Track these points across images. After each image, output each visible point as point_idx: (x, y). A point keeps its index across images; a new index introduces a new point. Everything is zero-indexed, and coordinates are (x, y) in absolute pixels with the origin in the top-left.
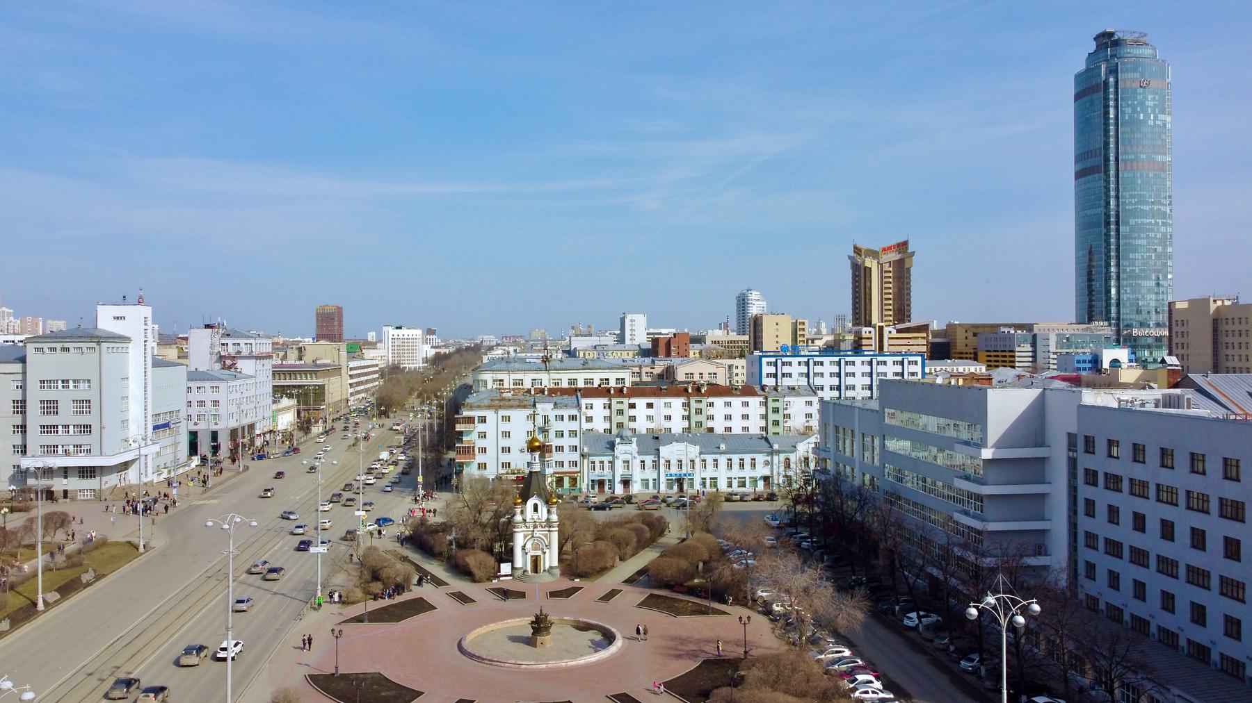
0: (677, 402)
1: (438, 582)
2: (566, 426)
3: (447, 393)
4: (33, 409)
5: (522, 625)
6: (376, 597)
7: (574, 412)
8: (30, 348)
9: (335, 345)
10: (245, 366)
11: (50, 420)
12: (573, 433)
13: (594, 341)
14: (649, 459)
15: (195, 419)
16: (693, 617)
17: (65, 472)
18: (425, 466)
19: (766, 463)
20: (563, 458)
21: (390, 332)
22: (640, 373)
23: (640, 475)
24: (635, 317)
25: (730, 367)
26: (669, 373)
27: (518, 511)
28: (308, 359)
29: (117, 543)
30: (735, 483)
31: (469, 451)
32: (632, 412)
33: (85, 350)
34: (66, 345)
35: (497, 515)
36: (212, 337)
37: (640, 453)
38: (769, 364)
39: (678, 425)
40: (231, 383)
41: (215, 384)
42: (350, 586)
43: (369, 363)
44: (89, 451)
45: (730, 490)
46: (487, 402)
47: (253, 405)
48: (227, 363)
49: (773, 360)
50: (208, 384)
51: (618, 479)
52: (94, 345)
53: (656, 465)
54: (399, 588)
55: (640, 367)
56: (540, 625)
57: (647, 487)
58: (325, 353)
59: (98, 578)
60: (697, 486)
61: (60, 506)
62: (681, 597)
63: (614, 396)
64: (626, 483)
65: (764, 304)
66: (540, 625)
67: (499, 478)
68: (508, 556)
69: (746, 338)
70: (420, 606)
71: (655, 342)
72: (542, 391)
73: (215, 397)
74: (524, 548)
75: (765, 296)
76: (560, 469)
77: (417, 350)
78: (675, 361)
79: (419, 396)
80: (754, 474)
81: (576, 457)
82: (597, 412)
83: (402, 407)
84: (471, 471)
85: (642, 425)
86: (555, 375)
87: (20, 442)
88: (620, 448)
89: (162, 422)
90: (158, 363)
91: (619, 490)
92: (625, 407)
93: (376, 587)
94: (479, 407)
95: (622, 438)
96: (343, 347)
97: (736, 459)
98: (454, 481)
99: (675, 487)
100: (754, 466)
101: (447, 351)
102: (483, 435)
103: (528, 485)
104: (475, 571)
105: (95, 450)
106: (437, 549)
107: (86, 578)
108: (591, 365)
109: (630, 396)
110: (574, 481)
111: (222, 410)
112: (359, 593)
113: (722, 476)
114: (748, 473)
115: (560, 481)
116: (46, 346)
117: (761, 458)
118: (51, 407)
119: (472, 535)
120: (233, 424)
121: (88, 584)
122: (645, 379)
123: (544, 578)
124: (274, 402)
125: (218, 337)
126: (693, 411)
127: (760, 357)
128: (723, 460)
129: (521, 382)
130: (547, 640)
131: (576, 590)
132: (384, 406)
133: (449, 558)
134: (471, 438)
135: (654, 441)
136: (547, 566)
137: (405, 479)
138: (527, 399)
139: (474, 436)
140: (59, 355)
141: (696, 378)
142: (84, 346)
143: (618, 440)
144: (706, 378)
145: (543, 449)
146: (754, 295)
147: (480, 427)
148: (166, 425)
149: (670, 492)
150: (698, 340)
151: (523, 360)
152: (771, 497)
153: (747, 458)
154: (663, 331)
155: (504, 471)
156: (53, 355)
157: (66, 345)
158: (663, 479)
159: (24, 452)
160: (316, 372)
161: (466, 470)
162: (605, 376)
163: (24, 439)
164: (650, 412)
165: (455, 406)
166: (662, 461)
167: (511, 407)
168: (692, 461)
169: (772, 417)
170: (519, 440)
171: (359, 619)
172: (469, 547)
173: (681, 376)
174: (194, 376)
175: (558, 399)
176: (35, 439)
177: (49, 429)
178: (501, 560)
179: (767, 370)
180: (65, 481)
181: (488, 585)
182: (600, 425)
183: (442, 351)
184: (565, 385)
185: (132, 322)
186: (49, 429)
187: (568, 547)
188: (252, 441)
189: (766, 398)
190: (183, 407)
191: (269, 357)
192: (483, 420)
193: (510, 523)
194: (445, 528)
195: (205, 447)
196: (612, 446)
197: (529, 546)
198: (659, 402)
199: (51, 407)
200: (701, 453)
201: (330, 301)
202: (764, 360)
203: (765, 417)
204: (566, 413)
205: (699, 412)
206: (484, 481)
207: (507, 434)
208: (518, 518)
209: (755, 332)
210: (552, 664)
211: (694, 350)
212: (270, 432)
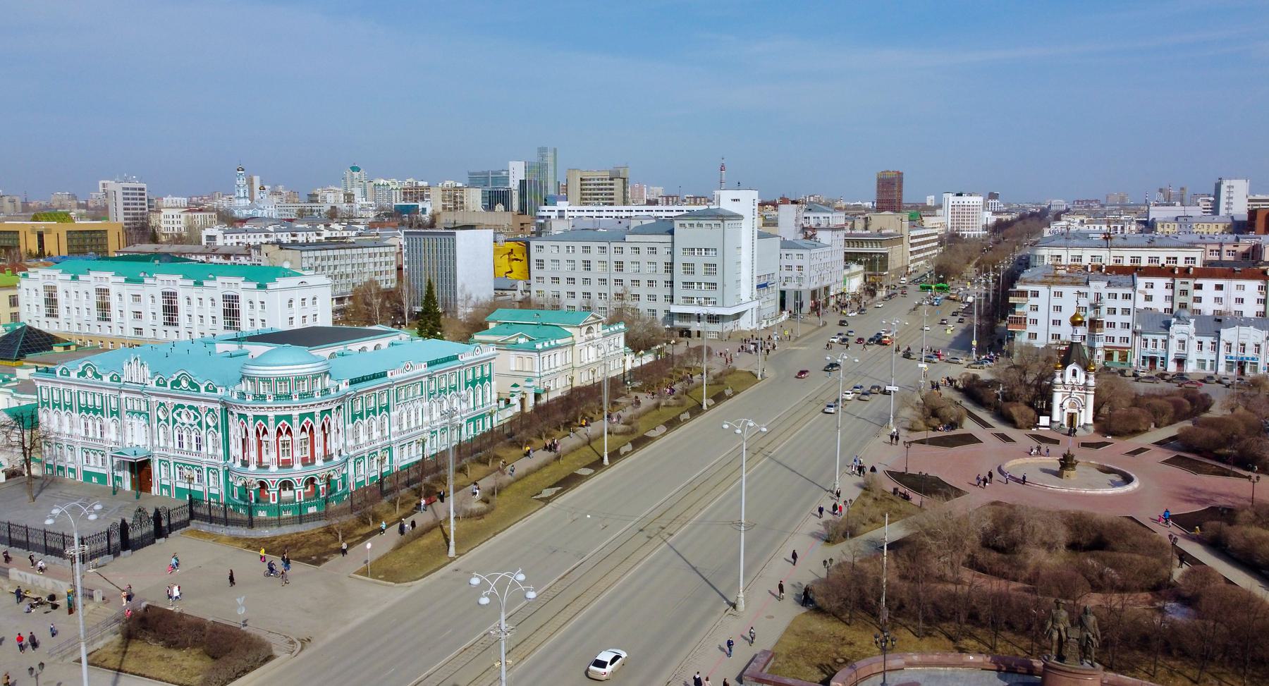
1: (985, 425)
2: (1120, 304)
3: (1005, 265)
4: (678, 269)
5: (1053, 462)
6: (935, 429)
7: (1128, 291)
8: (677, 223)
9: (899, 215)
10: (823, 236)
11: (689, 278)
12: (1126, 311)
13: (1177, 210)
14: (1207, 341)
18: (980, 332)
20: (1115, 333)
21: (951, 199)
22: (1220, 252)
23: (1196, 355)
24: (1234, 182)
27: (1058, 374)
28: (873, 228)
29: (742, 372)
31: (1021, 321)
32: (1197, 293)
35: (1041, 378)
36: (797, 211)
37: (1197, 334)
39: (1251, 308)
40: (813, 251)
41: (800, 252)
42: (916, 419)
43: (929, 231)
44: (715, 303)
46: (1040, 278)
48: (809, 233)
50: (794, 252)
51: (1171, 357)
53: (1215, 347)
54: (953, 425)
55: (1221, 245)
56: (1067, 462)
57: (1203, 367)
58: (887, 222)
59: (735, 393)
61: (694, 343)
62: (1207, 461)
64: (1180, 362)
66: (1067, 462)
67: (1048, 347)
68: (1048, 411)
70: (969, 439)
71: (1253, 214)
72: (1100, 269)
73: (800, 262)
74: (1061, 405)
76: (1110, 344)
77: (976, 215)
79: (977, 265)
81: (1128, 333)
82: (1159, 293)
83: (959, 274)
84: (1022, 339)
85: (1208, 307)
86: (1115, 252)
87: (669, 294)
88: (1175, 328)
89: (762, 282)
90: (761, 236)
91: (1172, 368)
93: (935, 422)
94: (1032, 282)
95: (1178, 318)
96: (906, 216)
98: (1005, 347)
99: (1235, 370)
101: (1009, 218)
102: (1035, 308)
103: (1070, 354)
104: (1017, 419)
105: (719, 303)
106: (987, 400)
107: (728, 392)
108: (1157, 242)
110: (1124, 357)
111: (805, 272)
112: (921, 424)
115: (1109, 356)
116: (687, 223)
118: (689, 268)
119: (1016, 391)
120: (813, 286)
121: (730, 397)
122: (1226, 257)
124: (846, 267)
130: (1072, 474)
131: (1106, 444)
132: (943, 274)
133: (996, 408)
134: (1024, 308)
137: (961, 344)
138: (1079, 276)
139: (1026, 309)
142: (713, 222)
145: (1094, 324)
147: (1033, 301)
148: (765, 285)
149: (1229, 374)
151: (1086, 236)
155: (1054, 342)
158: (1222, 360)
159: (672, 301)
160: (880, 241)
161: (1018, 338)
162: (1172, 255)
163: (672, 291)
164: (1219, 294)
165: (1012, 278)
166: (1222, 344)
167: (1063, 284)
171: (922, 442)
172: (1017, 399)
174: (786, 245)
175: (1113, 278)
177: (688, 285)
178: (1041, 413)
181: (1028, 432)
182: (1160, 304)
183: (1005, 217)
184: (1127, 263)
185: (743, 202)
186: (688, 285)
187: (1105, 410)
191: (841, 228)
193: (1050, 388)
194: (993, 384)
195: (790, 304)
196: (1167, 325)
197: (1066, 404)
198: (1230, 285)
199: (689, 268)
201: (892, 167)
206: (1030, 348)
207: (1059, 308)
208: (1058, 380)
210: (1073, 490)
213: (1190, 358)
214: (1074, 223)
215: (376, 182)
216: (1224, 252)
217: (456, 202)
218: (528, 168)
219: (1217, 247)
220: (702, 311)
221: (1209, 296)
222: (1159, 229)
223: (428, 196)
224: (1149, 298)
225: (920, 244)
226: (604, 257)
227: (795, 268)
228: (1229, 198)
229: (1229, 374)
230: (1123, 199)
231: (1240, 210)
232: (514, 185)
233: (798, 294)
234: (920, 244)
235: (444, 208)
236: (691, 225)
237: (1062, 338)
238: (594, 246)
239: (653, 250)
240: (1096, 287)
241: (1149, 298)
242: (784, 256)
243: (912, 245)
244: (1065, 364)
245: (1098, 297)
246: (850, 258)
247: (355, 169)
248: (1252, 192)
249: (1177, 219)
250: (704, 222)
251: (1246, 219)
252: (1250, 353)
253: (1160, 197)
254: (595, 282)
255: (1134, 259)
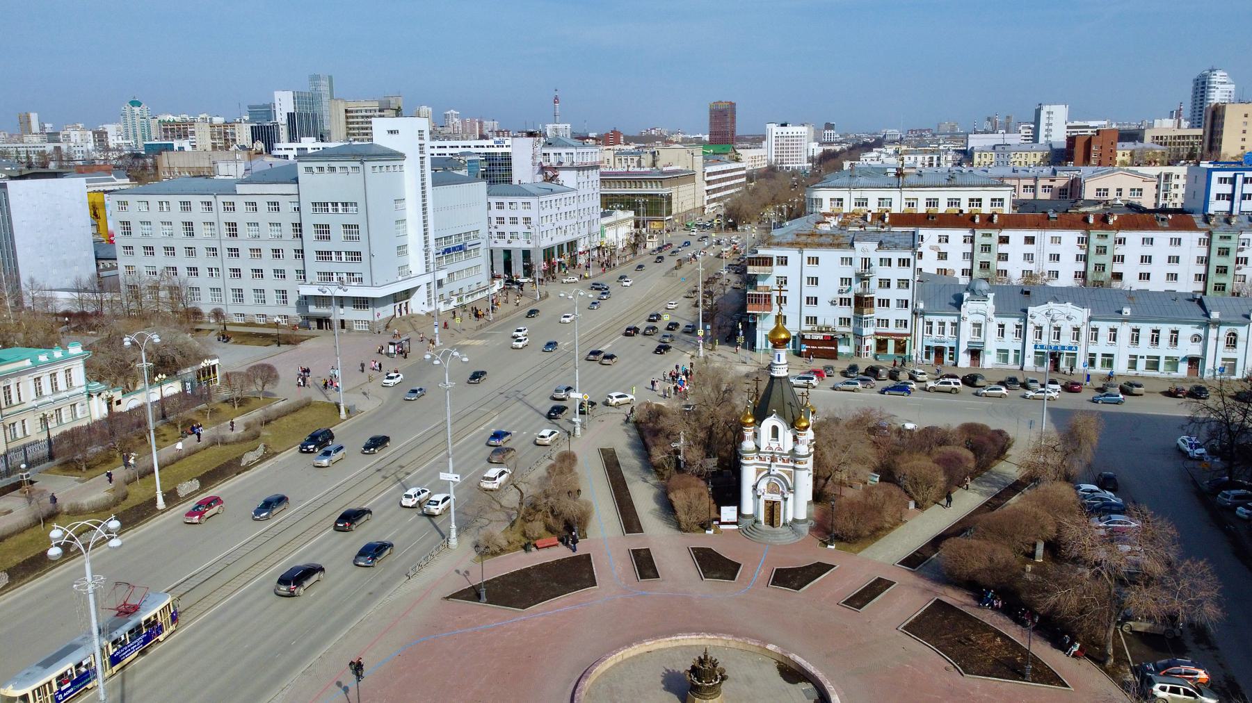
0: (1070, 238)
1: (631, 522)
2: (895, 273)
4: (309, 233)
7: (907, 255)
8: (301, 167)
10: (567, 178)
11: (324, 246)
12: (903, 283)
14: (1011, 323)
15: (508, 236)
16: (994, 681)
17: (342, 301)
19: (1196, 339)
21: (774, 130)
22: (1034, 188)
24: (1053, 108)
25: (1167, 176)
26: (1073, 191)
27: (749, 433)
30: (1141, 364)
32: (1003, 248)
33: (350, 169)
34: (333, 164)
38: (1222, 180)
40: (543, 199)
41: (526, 199)
44: (361, 280)
45: (1132, 372)
46: (790, 238)
47: (574, 221)
49: (1230, 174)
50: (519, 200)
51: (963, 347)
52: (357, 164)
53: (1021, 332)
55: (1036, 179)
57: (1005, 359)
60: (1080, 365)
63: (981, 226)
64: (975, 353)
65: (1232, 87)
68: (734, 498)
69: (1199, 132)
71: (1071, 140)
73: (527, 213)
74: (755, 487)
75: (1234, 77)
78: (1085, 171)
80: (1173, 353)
81: (906, 314)
82: (947, 252)
86: (908, 194)
88: (969, 307)
91: (964, 361)
92: (994, 241)
94: (779, 244)
95: (973, 292)
97: (1146, 330)
99: (1048, 365)
100: (1174, 340)
101: (838, 148)
102: (783, 281)
105: (366, 281)
108: (959, 180)
109: (1001, 226)
110: (901, 347)
113: (1122, 352)
114: (1164, 350)
115: (881, 345)
117: (1186, 331)
118: (323, 232)
120: (546, 243)
121: (247, 468)
122: (1043, 195)
123: (784, 536)
124: (604, 215)
125: (539, 146)
126: (1093, 249)
127: (1210, 171)
128: (1125, 330)
129: (862, 202)
131: (821, 568)
135: (1023, 297)
136: (790, 518)
139: (771, 282)
140: (326, 175)
141: (1112, 195)
142: (349, 164)
143: (967, 295)
144: (1126, 195)
145: (861, 303)
146: (1218, 77)
147: (778, 270)
148: (461, 248)
150: (1132, 136)
152: (1197, 393)
153: (1165, 330)
154: (1092, 124)
156: (321, 176)
157: (333, 164)
158: (1030, 350)
160: (661, 180)
162: (976, 195)
164: (1030, 249)
166: (1030, 327)
168: (1077, 329)
169: (1216, 261)
170: (829, 289)
173: (1089, 193)
176: (314, 266)
177: (324, 255)
179: (1216, 188)
180: (342, 311)
186: (324, 255)
188: (574, 260)
189: (1210, 234)
190: (484, 231)
192: (784, 261)
196: (958, 302)
197: (763, 486)
198: (1044, 237)
199: (323, 232)
200: (1090, 319)
201: (723, 95)
202: (1216, 176)
203: (1206, 261)
204: (895, 256)
205: (1102, 250)
207: (814, 281)
208: (748, 444)
209: (1212, 126)
211: (1122, 153)
212: (598, 248)
213: (988, 348)
214: (883, 158)
215: (161, 118)
216: (1039, 189)
217: (227, 140)
218: (298, 99)
219: (1031, 183)
220: (354, 291)
221: (1019, 254)
222: (976, 159)
223: (193, 133)
224: (943, 256)
225: (720, 181)
226: (210, 217)
227: (521, 221)
228: (1049, 124)
229: (1040, 369)
230: (953, 128)
231: (1059, 137)
232: (282, 119)
233: (526, 254)
234: (720, 181)
235: (214, 147)
236: (321, 169)
237: (820, 322)
238: (196, 200)
239: (275, 206)
240: (863, 250)
241: (943, 256)
242: (494, 206)
243: (709, 183)
244: (760, 414)
245: (867, 263)
246: (609, 203)
247: (135, 103)
248: (1071, 118)
249: (994, 147)
250: (337, 165)
251: (1065, 146)
252: (1066, 340)
253: (988, 126)
254: (245, 253)
255: (932, 202)
